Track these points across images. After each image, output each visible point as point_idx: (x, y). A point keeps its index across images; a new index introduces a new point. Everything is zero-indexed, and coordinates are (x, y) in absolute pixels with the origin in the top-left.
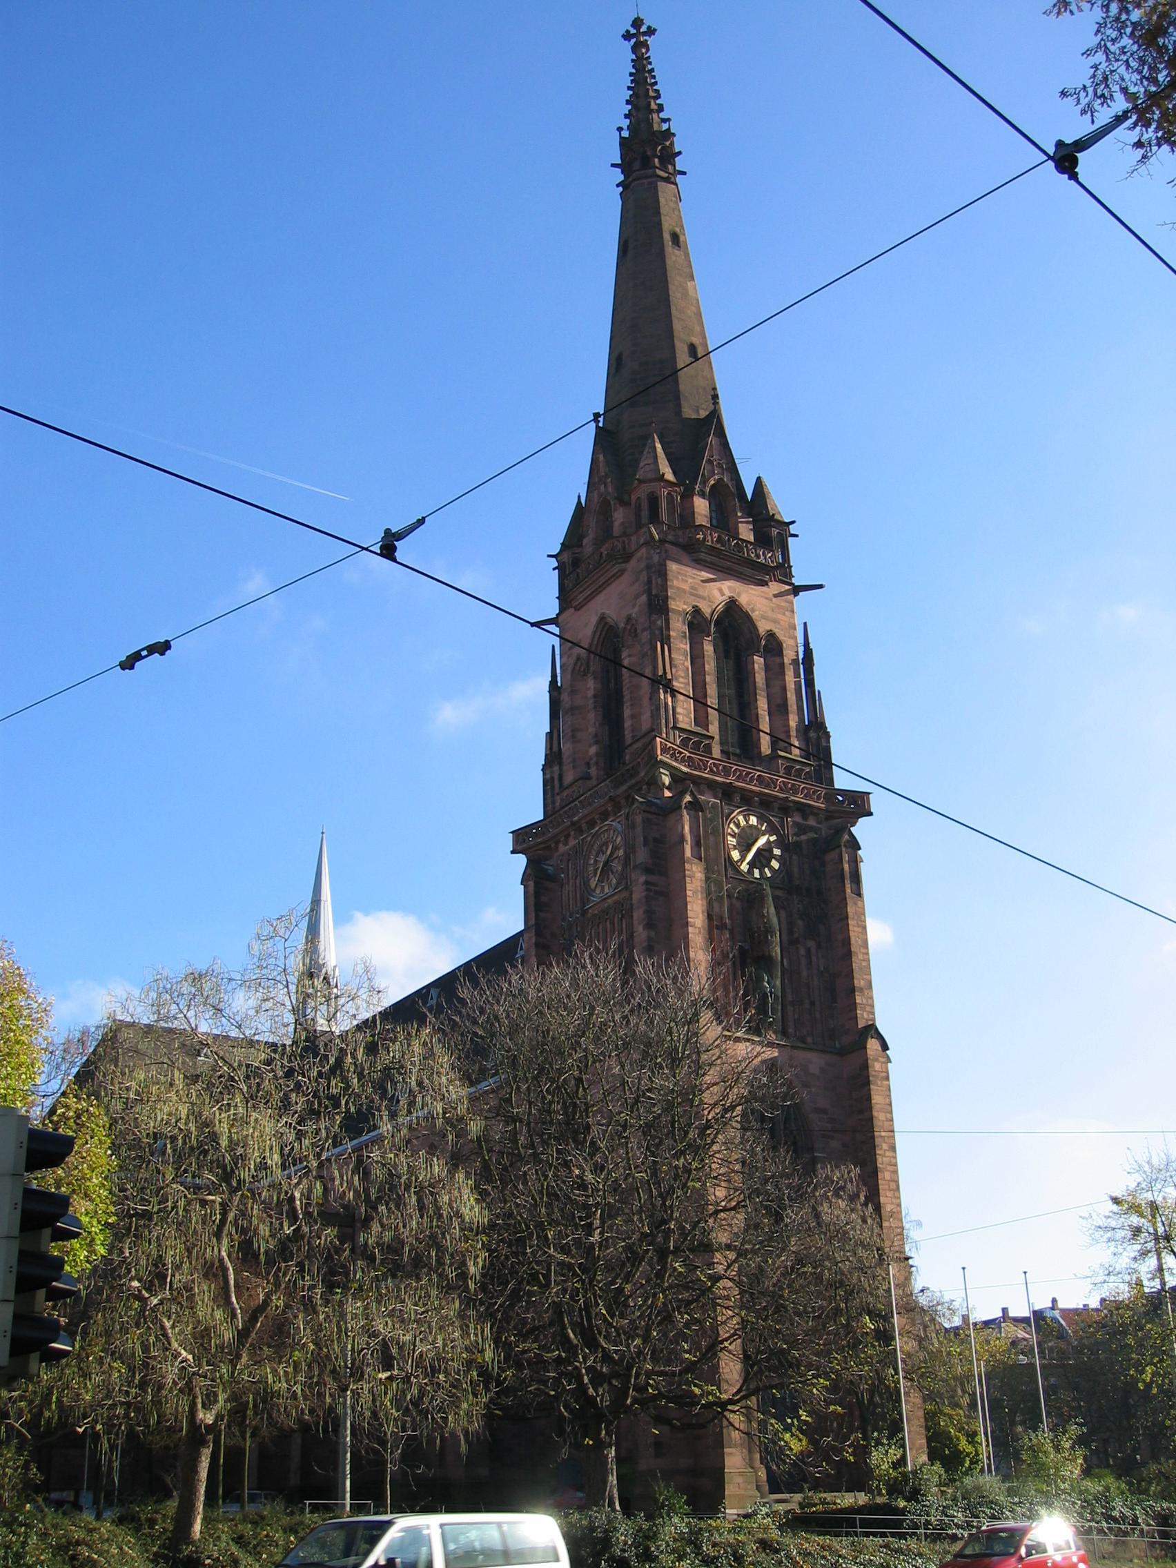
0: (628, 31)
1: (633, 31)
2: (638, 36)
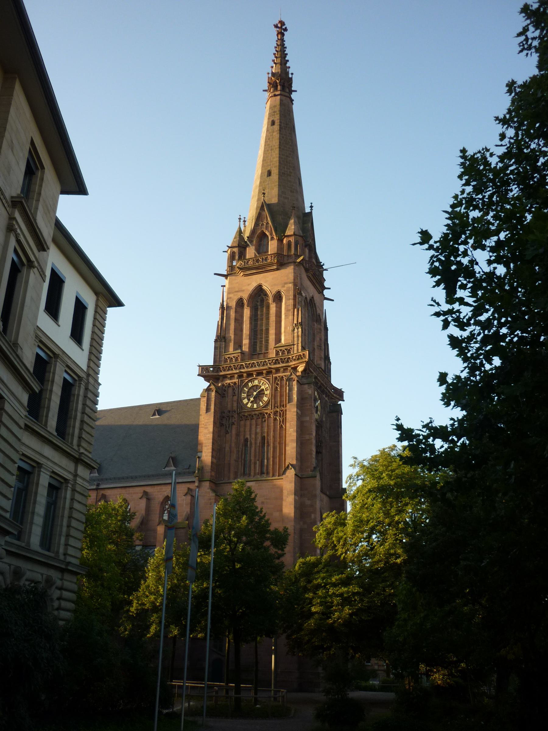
0: (277, 25)
1: (284, 27)
2: (329, 289)
